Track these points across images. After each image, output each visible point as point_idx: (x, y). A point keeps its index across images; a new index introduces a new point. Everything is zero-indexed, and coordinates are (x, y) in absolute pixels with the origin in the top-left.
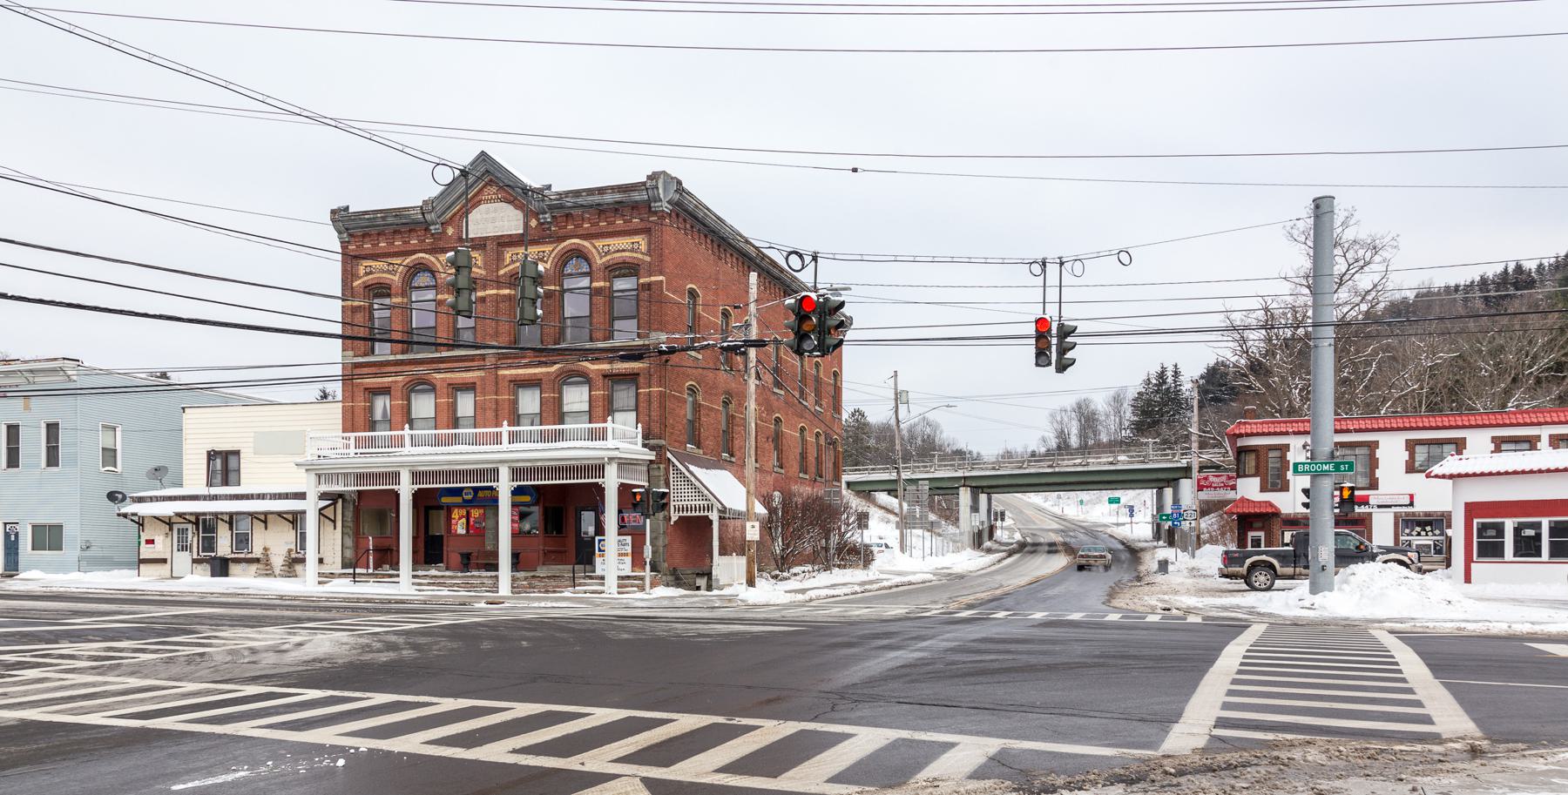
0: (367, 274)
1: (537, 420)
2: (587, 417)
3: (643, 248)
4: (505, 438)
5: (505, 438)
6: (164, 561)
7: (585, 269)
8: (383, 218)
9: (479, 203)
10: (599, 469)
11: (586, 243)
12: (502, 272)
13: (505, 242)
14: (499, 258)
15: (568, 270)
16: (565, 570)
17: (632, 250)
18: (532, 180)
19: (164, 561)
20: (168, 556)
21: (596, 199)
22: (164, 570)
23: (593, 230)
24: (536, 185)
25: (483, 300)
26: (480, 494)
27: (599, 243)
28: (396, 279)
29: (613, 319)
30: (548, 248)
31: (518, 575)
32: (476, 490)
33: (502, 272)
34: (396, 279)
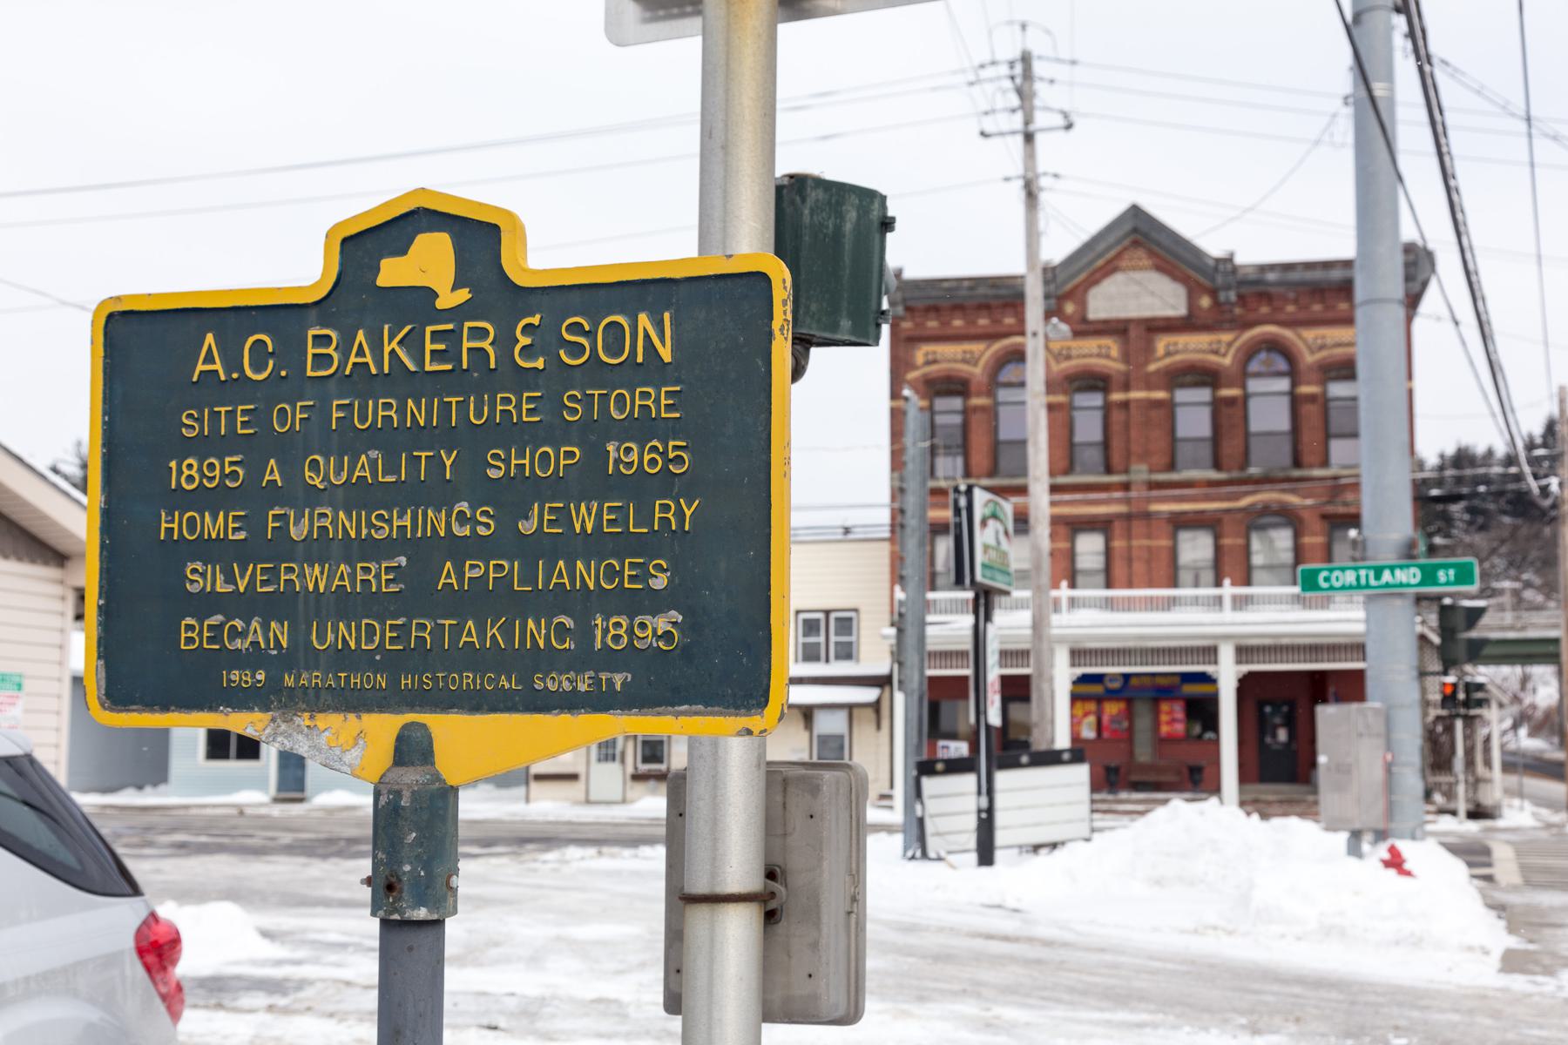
0: (928, 363)
1: (1209, 576)
2: (1101, 579)
3: (1115, 352)
4: (1227, 602)
5: (1227, 602)
6: (573, 777)
7: (1282, 365)
8: (971, 288)
9: (1115, 270)
10: (1210, 653)
11: (1287, 333)
12: (1152, 367)
13: (1157, 326)
14: (1149, 349)
15: (1254, 366)
16: (1286, 789)
17: (1099, 355)
18: (1213, 247)
19: (573, 777)
20: (580, 769)
21: (1317, 275)
22: (576, 789)
23: (1302, 316)
24: (299, 267)
25: (1125, 405)
26: (1134, 681)
27: (1310, 334)
28: (977, 372)
29: (1328, 436)
30: (1226, 337)
31: (1097, 796)
32: (1127, 677)
33: (1152, 367)
34: (977, 372)
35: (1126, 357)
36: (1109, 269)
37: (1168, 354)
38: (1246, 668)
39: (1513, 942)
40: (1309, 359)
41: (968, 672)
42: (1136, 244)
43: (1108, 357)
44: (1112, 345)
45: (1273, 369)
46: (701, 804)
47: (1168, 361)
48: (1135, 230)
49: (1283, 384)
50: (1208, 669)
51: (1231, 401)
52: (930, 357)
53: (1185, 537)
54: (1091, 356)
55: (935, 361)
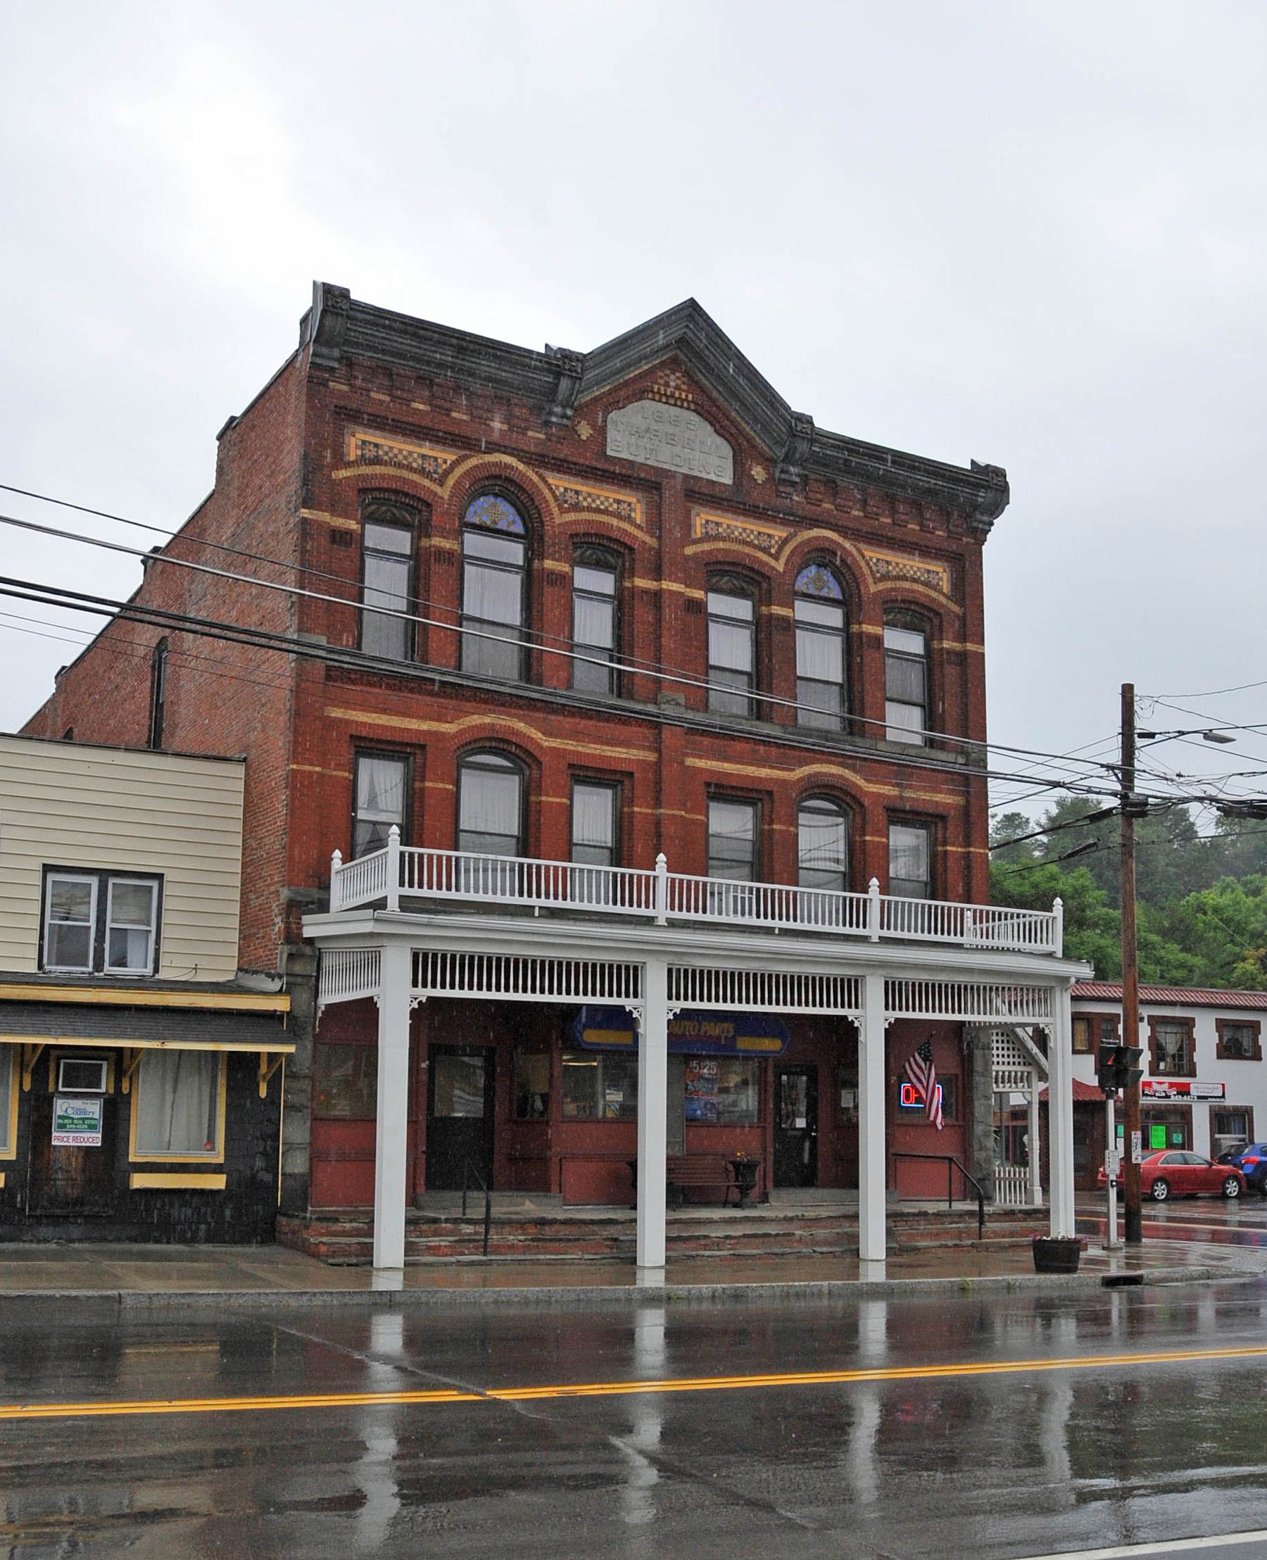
7: (507, 516)
12: (689, 551)
13: (699, 493)
35: (655, 523)
36: (638, 391)
37: (707, 538)
38: (894, 1015)
39: (617, 1441)
40: (559, 518)
41: (1118, 1009)
42: (674, 363)
43: (935, 588)
44: (635, 504)
45: (824, 593)
46: (424, 1148)
47: (706, 547)
48: (682, 342)
49: (834, 617)
50: (628, 1003)
51: (440, 554)
52: (370, 453)
53: (367, 767)
54: (606, 512)
55: (376, 461)
